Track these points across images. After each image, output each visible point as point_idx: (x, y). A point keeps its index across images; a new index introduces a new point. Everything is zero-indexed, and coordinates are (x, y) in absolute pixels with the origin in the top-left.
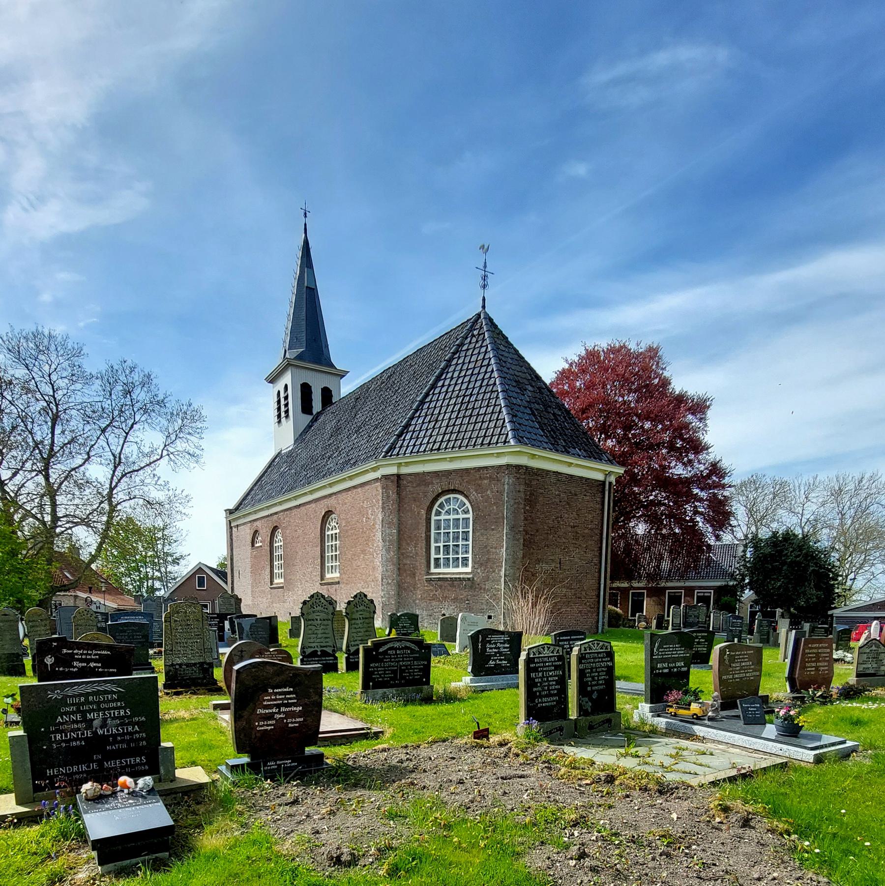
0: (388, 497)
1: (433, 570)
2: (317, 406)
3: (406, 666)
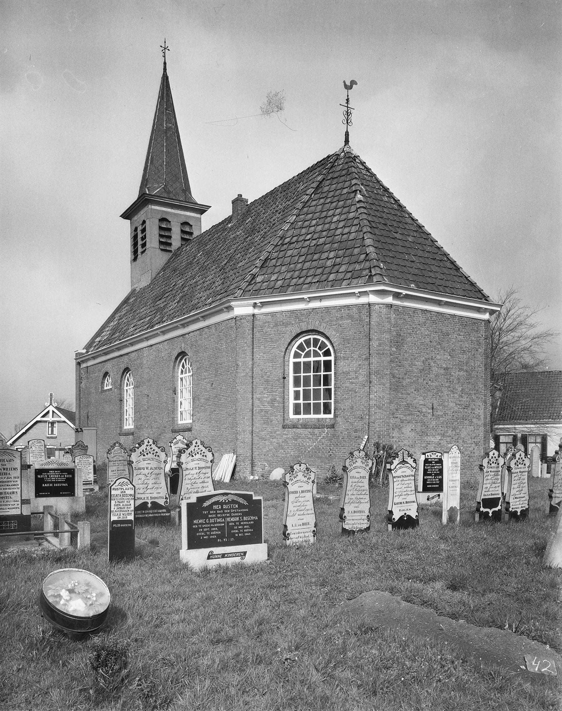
2: (176, 242)
3: (235, 522)
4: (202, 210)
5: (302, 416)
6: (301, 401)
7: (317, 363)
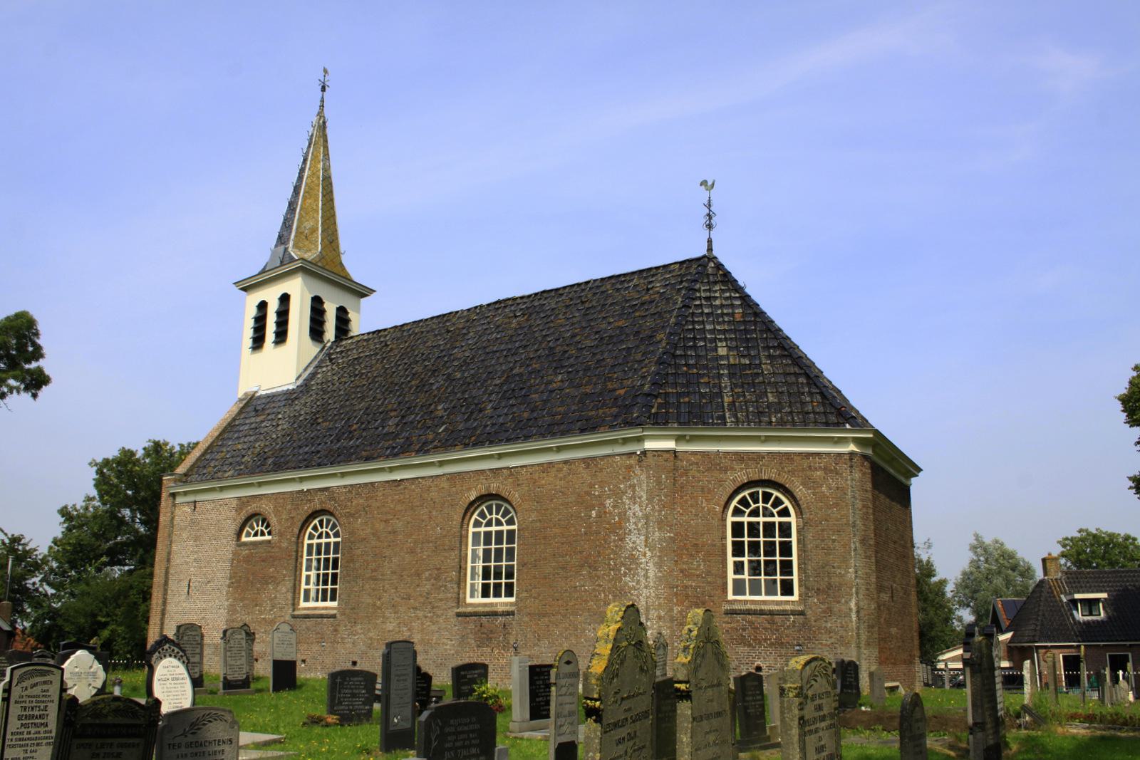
0: (659, 482)
4: (361, 292)
5: (491, 600)
6: (746, 576)
7: (499, 533)
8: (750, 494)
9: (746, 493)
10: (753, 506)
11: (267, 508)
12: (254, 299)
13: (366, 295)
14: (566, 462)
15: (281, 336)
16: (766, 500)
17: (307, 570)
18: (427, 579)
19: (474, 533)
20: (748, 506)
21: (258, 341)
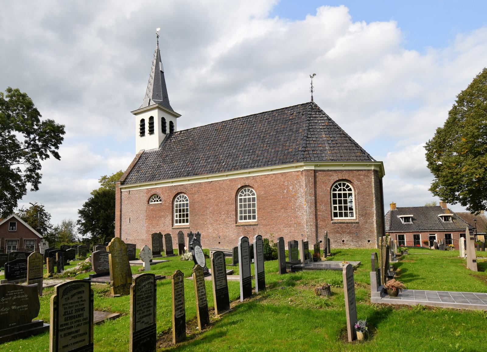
0: (309, 180)
1: (239, 221)
2: (168, 131)
4: (177, 116)
6: (338, 211)
8: (241, 193)
9: (337, 183)
10: (340, 188)
11: (159, 192)
12: (140, 117)
13: (179, 117)
14: (274, 174)
15: (151, 131)
16: (344, 186)
17: (176, 213)
18: (223, 215)
19: (176, 204)
20: (338, 188)
21: (142, 133)
